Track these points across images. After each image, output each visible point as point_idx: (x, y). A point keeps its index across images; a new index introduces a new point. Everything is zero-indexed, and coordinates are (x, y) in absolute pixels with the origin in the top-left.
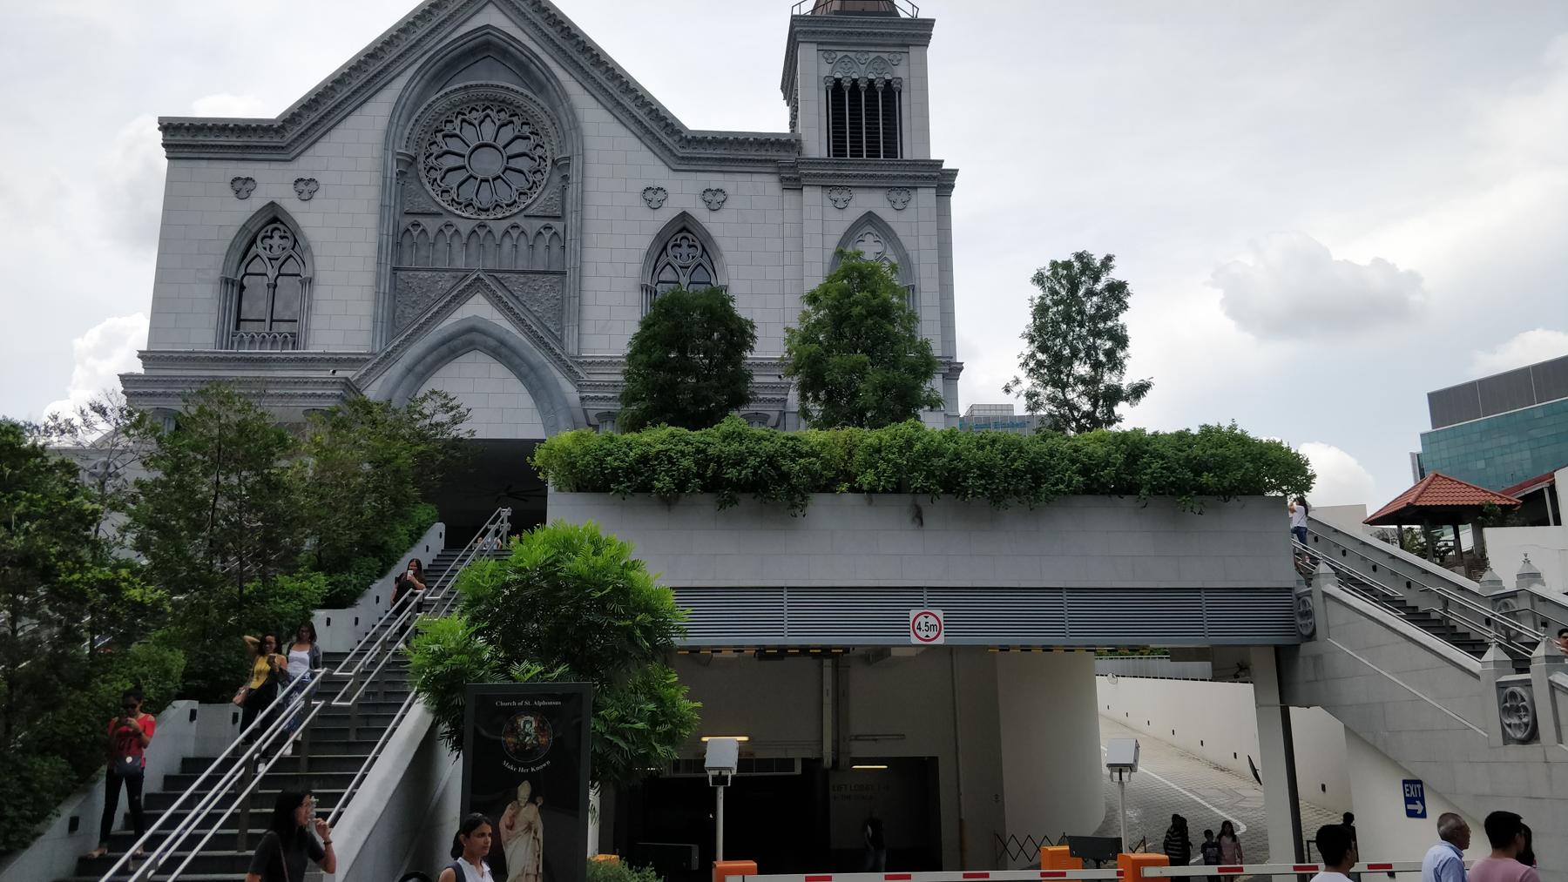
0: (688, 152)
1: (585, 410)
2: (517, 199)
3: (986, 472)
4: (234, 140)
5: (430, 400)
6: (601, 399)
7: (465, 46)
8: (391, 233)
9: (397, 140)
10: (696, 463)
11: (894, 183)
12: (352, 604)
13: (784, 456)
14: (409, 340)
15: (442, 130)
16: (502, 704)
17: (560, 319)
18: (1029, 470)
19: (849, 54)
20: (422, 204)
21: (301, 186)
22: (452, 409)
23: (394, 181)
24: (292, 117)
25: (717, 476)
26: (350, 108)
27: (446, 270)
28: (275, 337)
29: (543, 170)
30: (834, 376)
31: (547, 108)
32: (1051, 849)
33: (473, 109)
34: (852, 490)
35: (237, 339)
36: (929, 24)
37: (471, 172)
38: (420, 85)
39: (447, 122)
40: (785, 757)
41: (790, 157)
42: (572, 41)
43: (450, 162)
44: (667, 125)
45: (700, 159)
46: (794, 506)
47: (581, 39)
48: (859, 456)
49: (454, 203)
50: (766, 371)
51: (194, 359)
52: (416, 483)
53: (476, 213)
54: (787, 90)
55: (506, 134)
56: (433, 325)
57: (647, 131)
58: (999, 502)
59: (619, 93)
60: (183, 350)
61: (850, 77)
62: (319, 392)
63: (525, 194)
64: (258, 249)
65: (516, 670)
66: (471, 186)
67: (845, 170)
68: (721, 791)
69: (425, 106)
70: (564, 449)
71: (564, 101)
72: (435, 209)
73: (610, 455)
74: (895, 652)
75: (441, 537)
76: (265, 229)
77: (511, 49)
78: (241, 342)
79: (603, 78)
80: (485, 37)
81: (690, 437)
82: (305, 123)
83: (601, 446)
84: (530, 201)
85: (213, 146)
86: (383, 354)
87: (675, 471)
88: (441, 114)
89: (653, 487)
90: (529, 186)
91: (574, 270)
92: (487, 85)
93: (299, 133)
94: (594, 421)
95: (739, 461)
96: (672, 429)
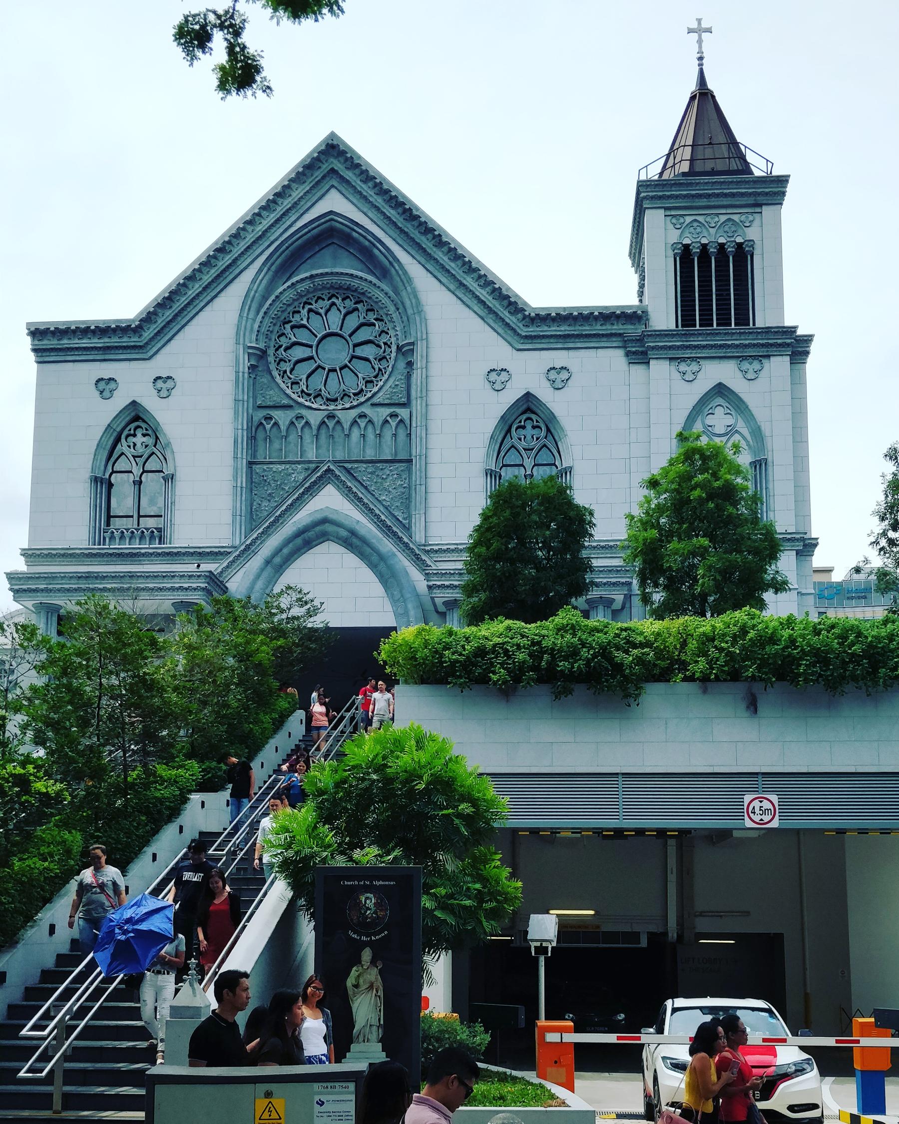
0: (532, 330)
1: (432, 598)
2: (364, 387)
3: (820, 656)
4: (96, 342)
5: (286, 595)
6: (448, 587)
7: (309, 235)
8: (245, 427)
9: (247, 334)
10: (530, 655)
11: (746, 352)
12: (224, 788)
13: (618, 648)
14: (266, 533)
15: (290, 321)
16: (346, 883)
17: (408, 507)
18: (866, 654)
19: (698, 218)
20: (274, 397)
21: (160, 384)
22: (306, 603)
23: (246, 375)
24: (149, 317)
25: (552, 664)
26: (202, 304)
27: (299, 463)
28: (143, 532)
29: (388, 357)
30: (673, 562)
31: (391, 293)
32: (861, 1020)
33: (319, 298)
34: (685, 679)
35: (108, 535)
36: (783, 181)
37: (319, 362)
38: (267, 277)
39: (294, 312)
40: (630, 930)
41: (639, 329)
42: (413, 223)
43: (299, 353)
44: (510, 303)
45: (544, 337)
46: (627, 696)
47: (423, 219)
48: (693, 645)
49: (303, 394)
50: (612, 554)
51: (71, 555)
52: (276, 676)
53: (324, 403)
54: (635, 258)
55: (352, 322)
56: (288, 517)
57: (490, 310)
58: (836, 688)
59: (462, 274)
60: (60, 547)
61: (700, 242)
62: (186, 585)
63: (372, 382)
64: (123, 447)
65: (357, 854)
66: (319, 377)
67: (694, 341)
68: (542, 960)
69: (273, 297)
70: (407, 644)
71: (407, 285)
72: (285, 401)
73: (449, 649)
74: (736, 834)
75: (301, 723)
76: (128, 428)
77: (355, 234)
78: (112, 537)
79: (446, 258)
80: (329, 223)
81: (526, 630)
82: (160, 321)
83: (441, 640)
84: (376, 389)
85: (77, 349)
86: (243, 547)
87: (510, 664)
88: (289, 305)
89: (490, 679)
90: (375, 374)
91: (420, 458)
92: (332, 273)
93: (155, 331)
94: (442, 609)
95: (573, 653)
96: (509, 622)
